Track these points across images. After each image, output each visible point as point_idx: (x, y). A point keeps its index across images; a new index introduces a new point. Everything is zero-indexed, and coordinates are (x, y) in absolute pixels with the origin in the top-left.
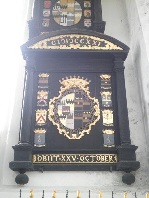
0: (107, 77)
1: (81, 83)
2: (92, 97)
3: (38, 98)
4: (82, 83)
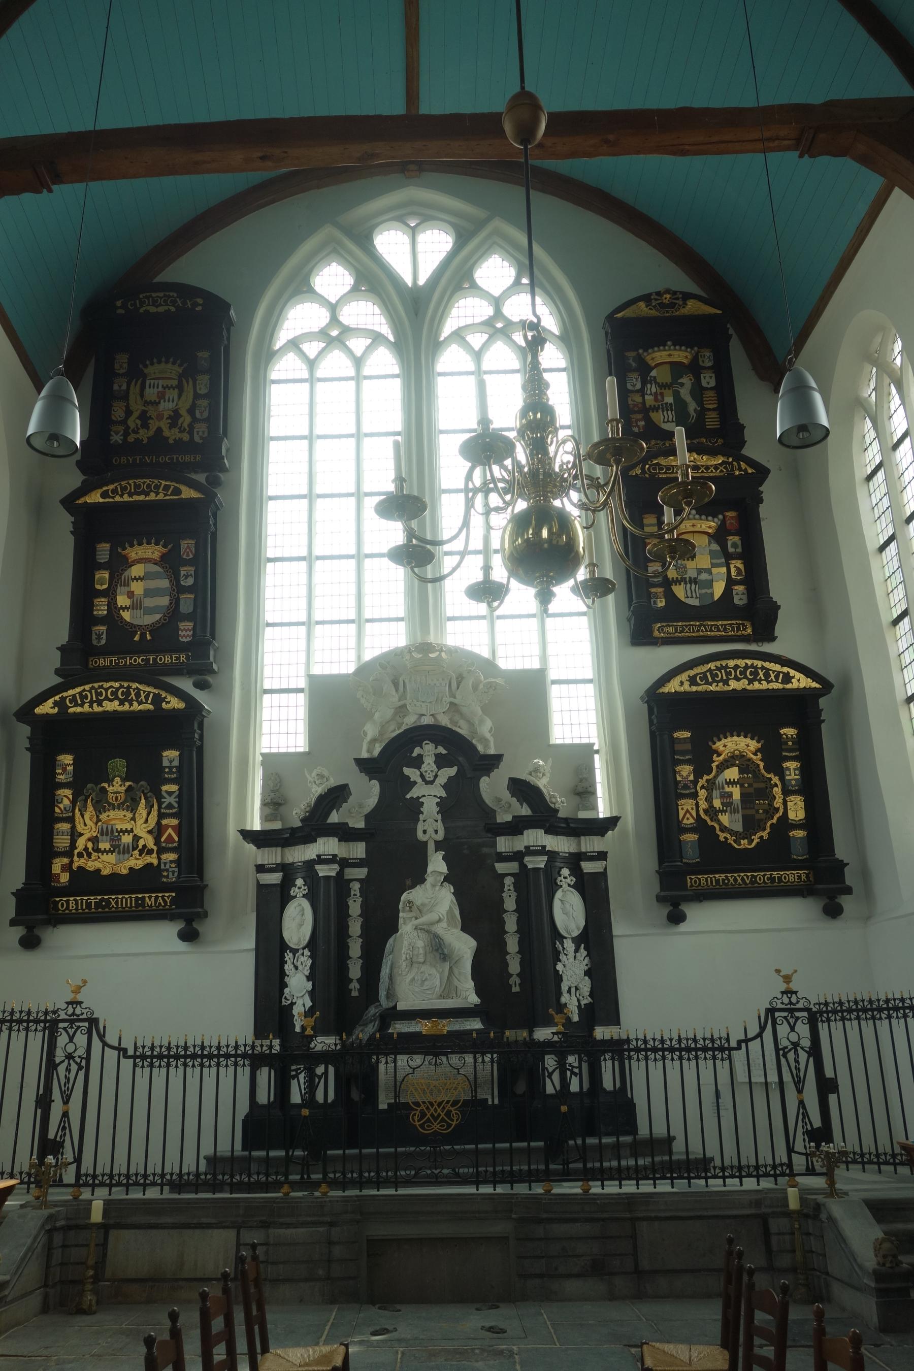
0: (790, 732)
1: (748, 746)
2: (769, 773)
3: (679, 778)
4: (745, 745)
